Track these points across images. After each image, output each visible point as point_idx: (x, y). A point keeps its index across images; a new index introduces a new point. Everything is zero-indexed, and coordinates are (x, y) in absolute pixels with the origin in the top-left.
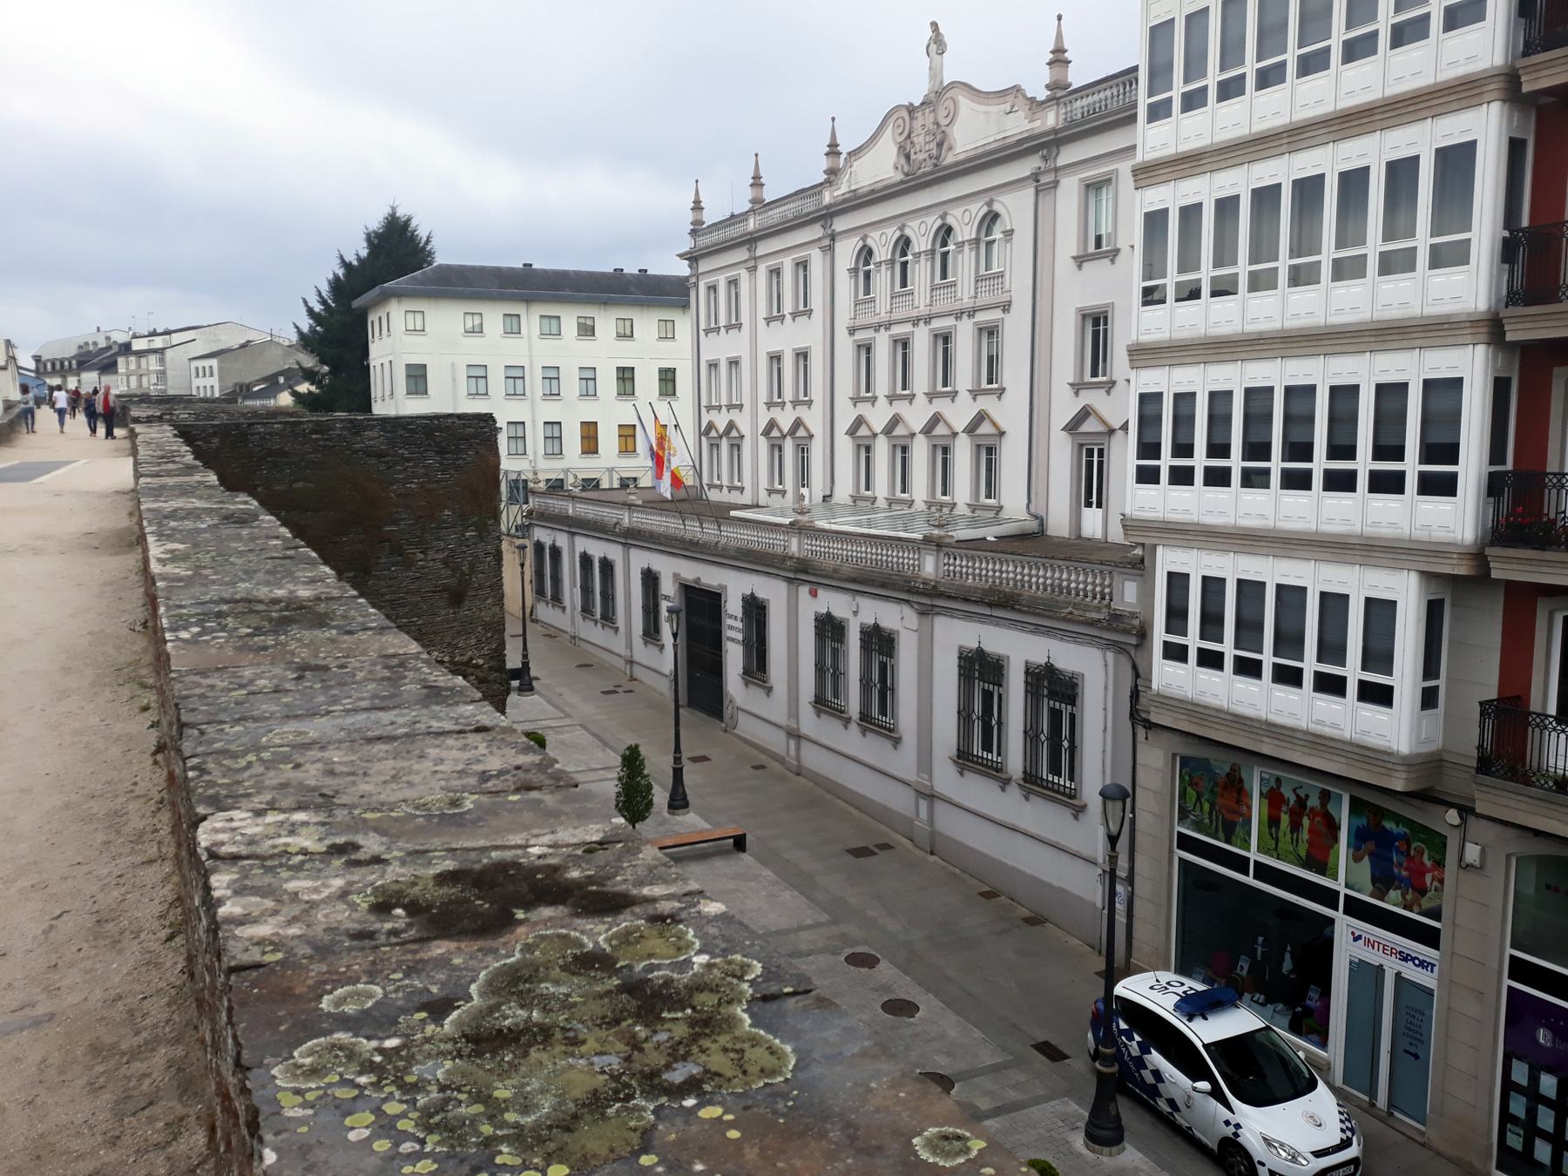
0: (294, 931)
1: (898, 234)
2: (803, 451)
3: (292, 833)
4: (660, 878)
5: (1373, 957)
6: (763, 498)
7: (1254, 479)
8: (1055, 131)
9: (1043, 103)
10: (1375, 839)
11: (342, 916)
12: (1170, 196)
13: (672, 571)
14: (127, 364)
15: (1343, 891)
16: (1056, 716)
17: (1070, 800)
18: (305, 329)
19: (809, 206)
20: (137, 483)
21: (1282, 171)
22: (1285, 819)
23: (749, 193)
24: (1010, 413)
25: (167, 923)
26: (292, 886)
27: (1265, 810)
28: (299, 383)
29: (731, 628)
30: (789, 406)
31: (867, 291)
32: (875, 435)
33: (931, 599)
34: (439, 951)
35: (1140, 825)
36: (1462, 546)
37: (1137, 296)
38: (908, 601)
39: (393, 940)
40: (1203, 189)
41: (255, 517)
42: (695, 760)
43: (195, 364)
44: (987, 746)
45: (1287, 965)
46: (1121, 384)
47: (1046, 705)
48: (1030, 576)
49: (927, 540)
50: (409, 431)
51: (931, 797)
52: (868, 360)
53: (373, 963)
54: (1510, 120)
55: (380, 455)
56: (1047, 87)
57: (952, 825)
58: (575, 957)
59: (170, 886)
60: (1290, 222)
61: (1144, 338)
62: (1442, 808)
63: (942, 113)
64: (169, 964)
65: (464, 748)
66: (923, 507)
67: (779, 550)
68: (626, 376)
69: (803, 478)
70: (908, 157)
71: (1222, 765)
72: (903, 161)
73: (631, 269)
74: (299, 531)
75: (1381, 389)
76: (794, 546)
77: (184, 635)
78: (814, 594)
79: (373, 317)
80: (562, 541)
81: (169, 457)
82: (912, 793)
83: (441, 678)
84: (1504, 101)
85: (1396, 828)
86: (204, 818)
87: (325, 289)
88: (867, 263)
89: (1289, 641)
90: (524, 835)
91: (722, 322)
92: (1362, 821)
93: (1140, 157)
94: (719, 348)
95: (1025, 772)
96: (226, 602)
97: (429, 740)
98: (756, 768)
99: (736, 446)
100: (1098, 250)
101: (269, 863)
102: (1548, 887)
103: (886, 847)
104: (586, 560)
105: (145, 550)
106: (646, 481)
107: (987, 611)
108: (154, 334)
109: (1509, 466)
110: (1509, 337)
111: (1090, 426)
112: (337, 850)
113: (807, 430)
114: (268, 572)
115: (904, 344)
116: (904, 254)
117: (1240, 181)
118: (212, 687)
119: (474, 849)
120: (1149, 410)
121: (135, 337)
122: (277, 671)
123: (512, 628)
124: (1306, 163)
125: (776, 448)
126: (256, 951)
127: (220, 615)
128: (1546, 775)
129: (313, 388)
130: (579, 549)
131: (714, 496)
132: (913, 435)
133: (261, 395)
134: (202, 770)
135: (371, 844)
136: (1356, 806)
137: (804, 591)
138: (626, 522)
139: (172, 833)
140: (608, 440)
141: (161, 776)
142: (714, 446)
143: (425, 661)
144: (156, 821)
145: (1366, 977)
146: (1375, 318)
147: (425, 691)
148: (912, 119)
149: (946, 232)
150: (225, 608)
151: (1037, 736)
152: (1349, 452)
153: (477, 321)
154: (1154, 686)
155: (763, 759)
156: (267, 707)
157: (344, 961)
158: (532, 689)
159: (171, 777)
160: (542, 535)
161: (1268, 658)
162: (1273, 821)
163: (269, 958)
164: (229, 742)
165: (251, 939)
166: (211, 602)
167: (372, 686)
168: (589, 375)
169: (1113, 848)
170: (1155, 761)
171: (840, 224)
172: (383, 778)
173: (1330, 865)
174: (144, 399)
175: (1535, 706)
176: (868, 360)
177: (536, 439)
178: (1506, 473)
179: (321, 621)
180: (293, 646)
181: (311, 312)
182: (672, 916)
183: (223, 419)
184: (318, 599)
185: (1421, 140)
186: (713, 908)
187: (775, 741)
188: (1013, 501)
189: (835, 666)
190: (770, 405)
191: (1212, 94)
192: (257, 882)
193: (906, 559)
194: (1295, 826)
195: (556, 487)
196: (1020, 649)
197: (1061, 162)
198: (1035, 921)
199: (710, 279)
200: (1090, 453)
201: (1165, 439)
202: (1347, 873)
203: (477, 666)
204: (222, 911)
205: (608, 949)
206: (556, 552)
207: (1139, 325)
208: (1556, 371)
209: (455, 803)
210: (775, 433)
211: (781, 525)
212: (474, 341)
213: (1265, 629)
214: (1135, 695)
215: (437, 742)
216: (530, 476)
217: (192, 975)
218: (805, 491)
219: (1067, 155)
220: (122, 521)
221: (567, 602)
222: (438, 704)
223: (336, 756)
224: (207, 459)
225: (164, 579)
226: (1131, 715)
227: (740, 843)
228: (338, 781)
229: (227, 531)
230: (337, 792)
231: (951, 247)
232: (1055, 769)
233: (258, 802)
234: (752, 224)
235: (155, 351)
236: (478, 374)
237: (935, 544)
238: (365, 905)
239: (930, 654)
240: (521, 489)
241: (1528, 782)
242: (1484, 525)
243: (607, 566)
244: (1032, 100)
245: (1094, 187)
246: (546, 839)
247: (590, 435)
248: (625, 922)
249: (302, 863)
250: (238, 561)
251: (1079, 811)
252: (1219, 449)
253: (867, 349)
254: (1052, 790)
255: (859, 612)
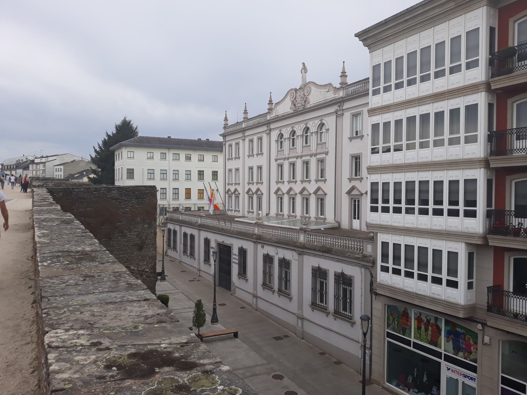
0: (76, 376)
1: (291, 129)
2: (260, 199)
3: (78, 338)
4: (207, 357)
5: (455, 376)
6: (246, 214)
7: (410, 211)
8: (342, 98)
9: (338, 89)
10: (454, 334)
11: (94, 370)
12: (380, 119)
13: (215, 239)
14: (33, 167)
15: (443, 352)
16: (345, 290)
17: (350, 320)
18: (94, 156)
19: (262, 120)
20: (33, 207)
21: (416, 111)
22: (423, 327)
23: (243, 116)
24: (328, 187)
25: (32, 366)
26: (77, 358)
27: (416, 323)
28: (90, 174)
29: (234, 258)
30: (255, 184)
31: (281, 147)
32: (284, 194)
33: (302, 249)
34: (128, 384)
35: (374, 329)
36: (479, 234)
37: (370, 151)
38: (294, 250)
39: (112, 379)
40: (391, 117)
41: (73, 221)
42: (220, 305)
43: (56, 167)
44: (322, 301)
45: (425, 379)
46: (365, 179)
47: (342, 286)
48: (336, 242)
49: (301, 229)
50: (127, 191)
51: (303, 319)
52: (281, 169)
53: (104, 388)
54: (487, 173)
55: (117, 199)
56: (340, 84)
57: (310, 329)
58: (176, 386)
59: (34, 353)
60: (419, 129)
61: (372, 165)
62: (476, 324)
63: (306, 91)
64: (32, 382)
65: (140, 307)
66: (299, 218)
67: (251, 232)
68: (201, 174)
69: (260, 208)
70: (295, 105)
71: (401, 308)
72: (293, 106)
73: (204, 139)
74: (88, 226)
75: (450, 182)
76: (256, 231)
77: (45, 264)
78: (263, 247)
79: (116, 153)
80: (177, 228)
81: (44, 200)
82: (296, 318)
83: (133, 280)
84: (488, 6)
85: (460, 330)
86: (47, 332)
87: (101, 143)
88: (281, 138)
89: (423, 266)
90: (159, 340)
91: (234, 156)
92: (449, 328)
93: (370, 107)
94: (232, 165)
95: (335, 310)
96: (61, 252)
97: (128, 304)
98: (242, 308)
99: (237, 197)
100: (357, 135)
101: (69, 350)
102: (513, 352)
103: (287, 336)
104: (185, 235)
105: (34, 233)
106: (206, 208)
107: (321, 254)
108: (42, 157)
109: (493, 208)
110: (491, 166)
111: (355, 192)
112: (94, 345)
113: (261, 192)
114: (76, 241)
115: (293, 165)
116: (293, 136)
117: (403, 115)
118: (54, 283)
119: (142, 345)
120: (374, 188)
121: (36, 158)
122: (77, 277)
123: (159, 258)
124: (424, 109)
125: (251, 198)
126: (62, 384)
127: (58, 256)
128: (510, 312)
129: (95, 176)
130: (183, 231)
131: (229, 213)
132: (296, 194)
133: (77, 178)
134: (48, 314)
135: (106, 342)
136: (447, 322)
137: (259, 246)
138: (199, 222)
139: (36, 333)
140: (194, 194)
141: (34, 312)
142: (230, 197)
143: (128, 274)
144: (31, 328)
145: (452, 383)
146: (448, 159)
147: (127, 285)
148: (296, 93)
149: (307, 129)
150: (60, 254)
151: (339, 298)
152: (441, 203)
153: (152, 154)
154: (378, 280)
155: (244, 305)
156: (72, 291)
157: (94, 387)
158: (165, 279)
159: (37, 313)
160: (171, 226)
161: (416, 272)
162: (419, 328)
163: (67, 387)
164: (58, 304)
165: (61, 379)
166: (56, 252)
167: (109, 283)
168: (189, 173)
169: (365, 337)
170: (379, 307)
171: (272, 126)
172: (111, 318)
173: (439, 343)
174: (38, 179)
175: (505, 288)
176: (281, 169)
177: (170, 194)
178: (493, 210)
179: (93, 259)
180: (83, 268)
181: (96, 151)
182: (210, 371)
183: (63, 186)
184: (92, 251)
185: (461, 103)
186: (225, 368)
187: (249, 299)
188: (330, 216)
189: (270, 273)
190: (249, 183)
191: (393, 87)
192: (64, 357)
193: (294, 235)
194: (426, 330)
195: (176, 210)
196: (332, 267)
197: (344, 108)
198: (338, 363)
199: (230, 143)
200: (355, 201)
201: (380, 198)
202: (444, 346)
203: (146, 272)
204: (51, 368)
205: (188, 383)
206: (175, 232)
207: (370, 160)
208: (507, 177)
209: (136, 327)
210: (250, 193)
211: (252, 223)
212: (150, 161)
213: (414, 261)
214: (372, 284)
215: (131, 304)
216: (168, 206)
217: (40, 387)
218: (260, 212)
219: (346, 105)
220: (28, 221)
221: (178, 249)
222: (131, 290)
223: (95, 309)
224: (57, 200)
225: (39, 243)
226: (371, 291)
227: (236, 335)
228: (96, 318)
229: (63, 226)
230: (95, 322)
231: (309, 134)
232: (345, 309)
233: (67, 326)
234: (244, 125)
235: (42, 163)
236: (151, 172)
237: (304, 231)
238: (102, 366)
239: (303, 268)
240: (164, 210)
241: (504, 315)
242: (486, 227)
243: (192, 237)
244: (335, 88)
245: (355, 116)
246: (167, 341)
247: (188, 193)
248: (194, 373)
249: (81, 349)
250: (66, 237)
251: (353, 324)
252: (397, 201)
253: (281, 166)
254: (344, 316)
255: (279, 254)
